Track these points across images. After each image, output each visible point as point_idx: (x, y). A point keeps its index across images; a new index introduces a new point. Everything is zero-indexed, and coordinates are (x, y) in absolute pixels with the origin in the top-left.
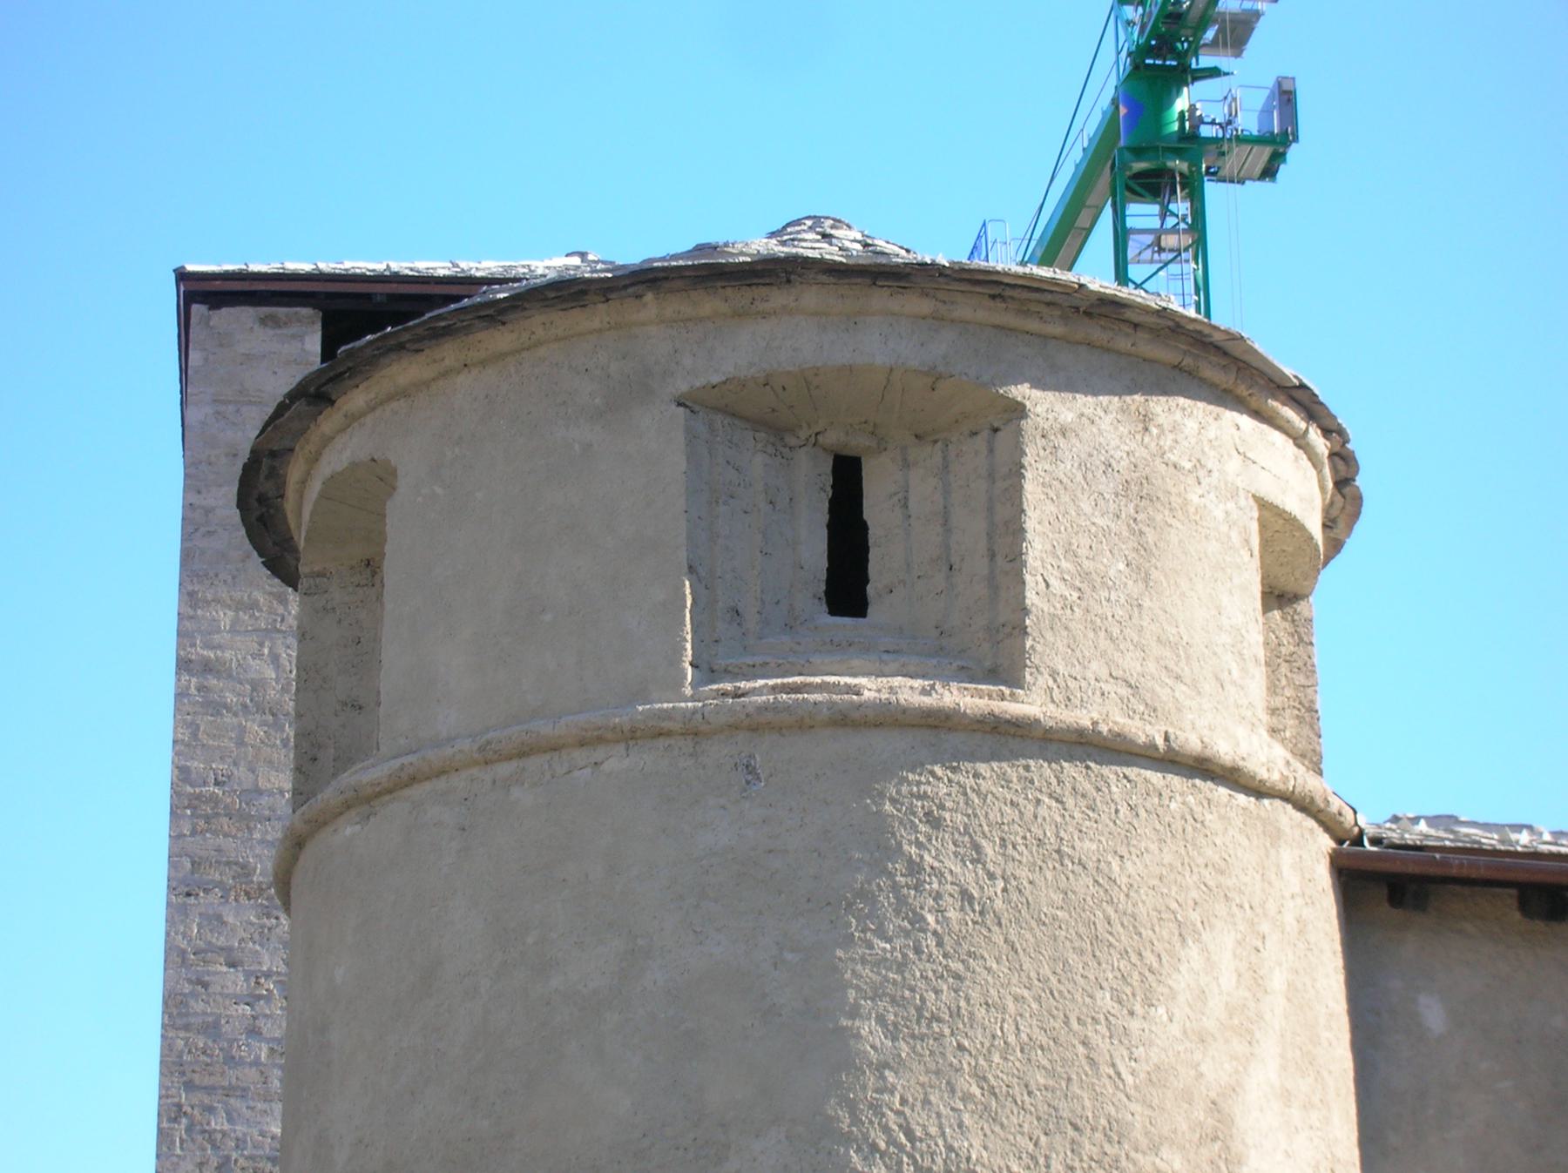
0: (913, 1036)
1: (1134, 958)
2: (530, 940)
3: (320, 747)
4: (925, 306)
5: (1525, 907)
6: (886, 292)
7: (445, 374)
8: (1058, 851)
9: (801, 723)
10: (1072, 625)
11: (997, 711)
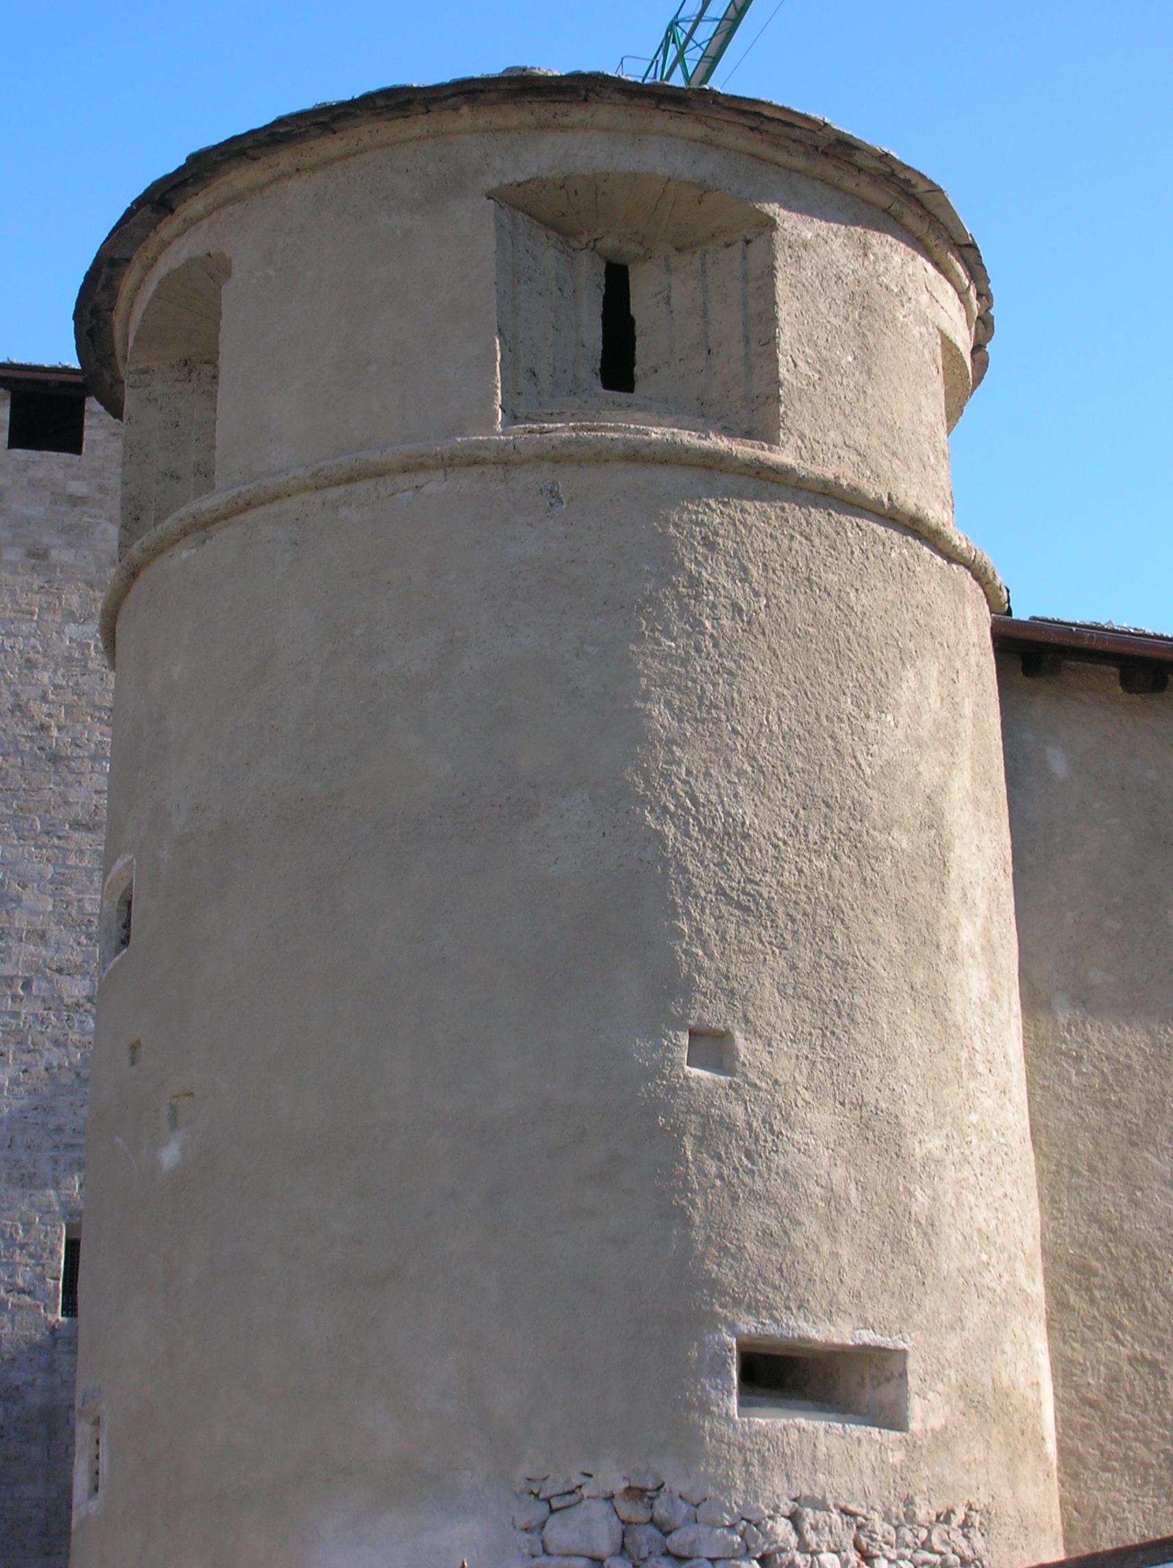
0: (696, 719)
1: (868, 673)
2: (358, 632)
3: (142, 509)
4: (698, 130)
5: (1127, 683)
6: (667, 115)
7: (276, 180)
8: (808, 579)
9: (600, 456)
10: (815, 399)
11: (761, 458)
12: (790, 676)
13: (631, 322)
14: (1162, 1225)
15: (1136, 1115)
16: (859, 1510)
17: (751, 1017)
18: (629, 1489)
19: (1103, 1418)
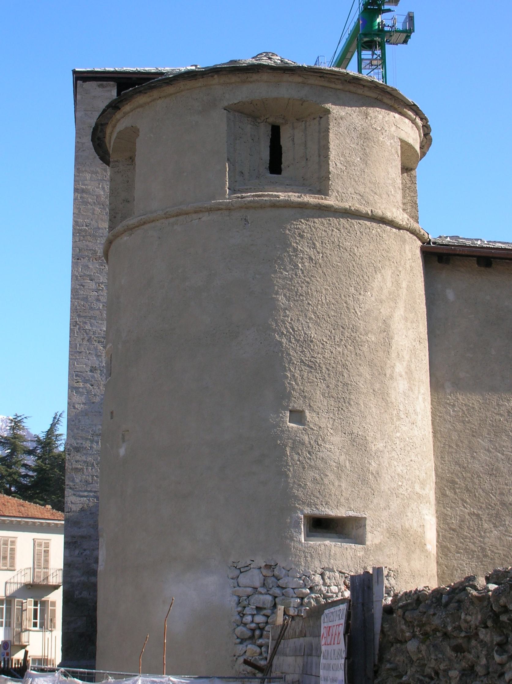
0: (294, 300)
1: (361, 278)
4: (300, 79)
5: (479, 263)
6: (288, 75)
8: (339, 245)
10: (344, 177)
12: (331, 282)
13: (280, 147)
14: (483, 465)
15: (475, 425)
16: (346, 572)
17: (312, 405)
18: (266, 565)
19: (457, 535)
